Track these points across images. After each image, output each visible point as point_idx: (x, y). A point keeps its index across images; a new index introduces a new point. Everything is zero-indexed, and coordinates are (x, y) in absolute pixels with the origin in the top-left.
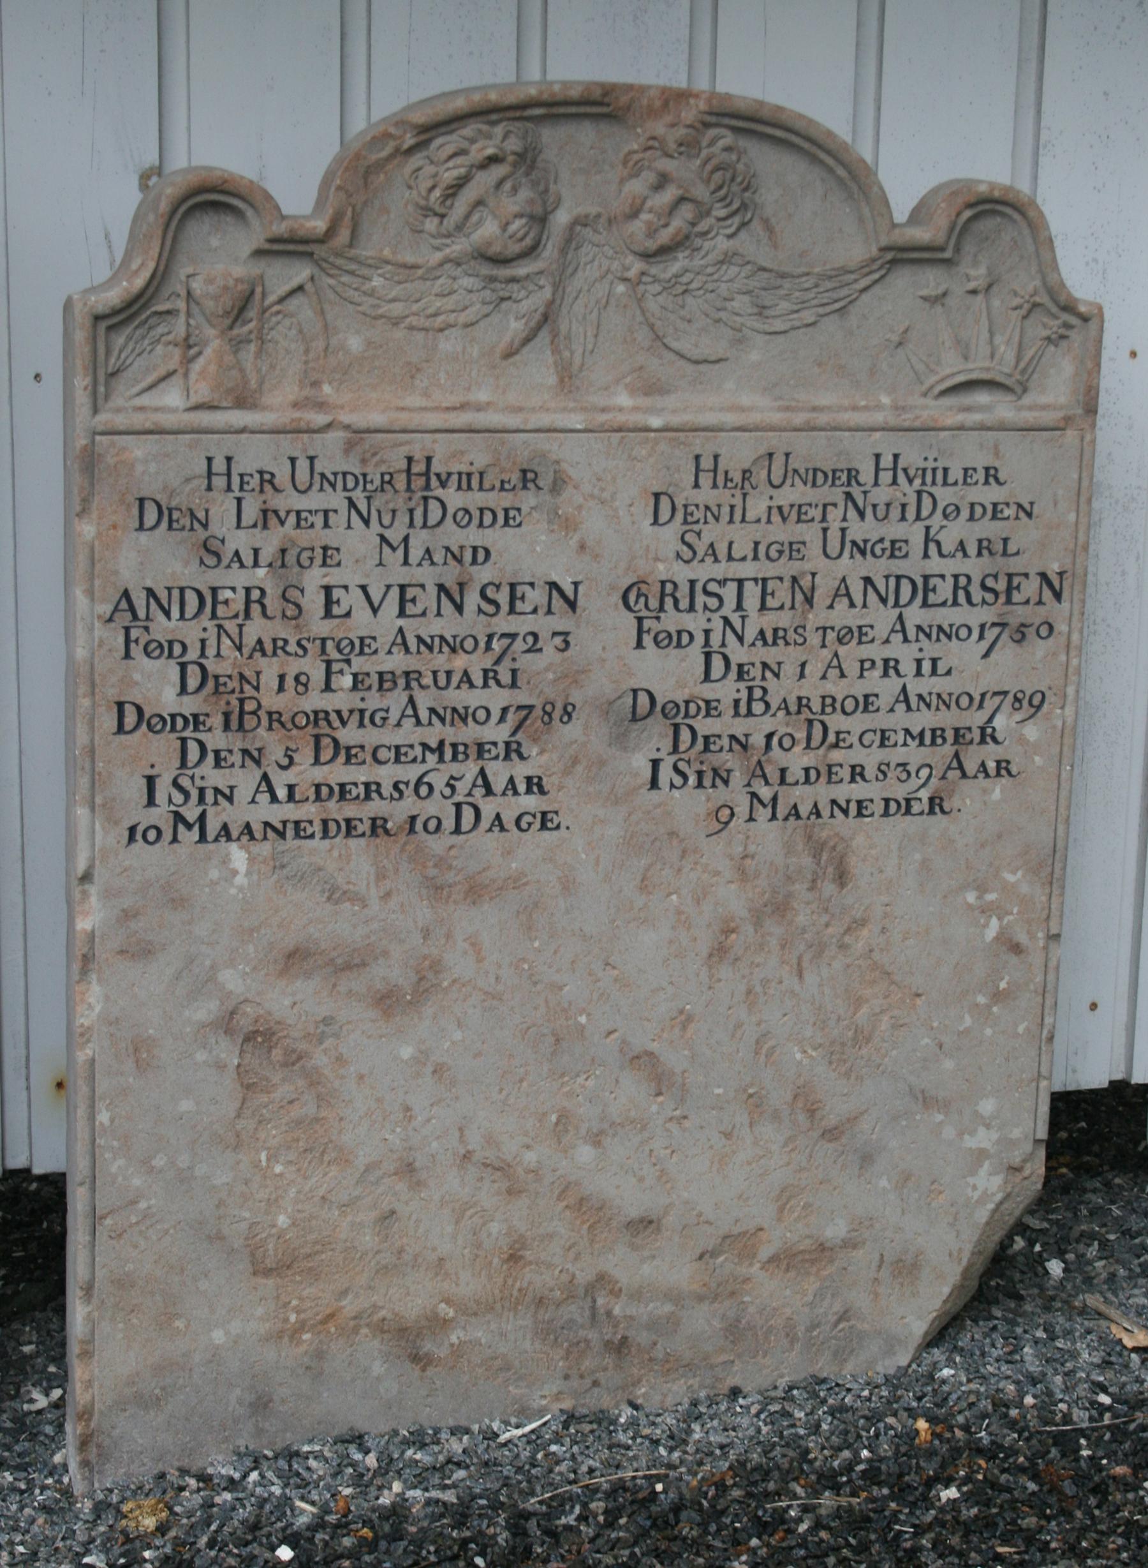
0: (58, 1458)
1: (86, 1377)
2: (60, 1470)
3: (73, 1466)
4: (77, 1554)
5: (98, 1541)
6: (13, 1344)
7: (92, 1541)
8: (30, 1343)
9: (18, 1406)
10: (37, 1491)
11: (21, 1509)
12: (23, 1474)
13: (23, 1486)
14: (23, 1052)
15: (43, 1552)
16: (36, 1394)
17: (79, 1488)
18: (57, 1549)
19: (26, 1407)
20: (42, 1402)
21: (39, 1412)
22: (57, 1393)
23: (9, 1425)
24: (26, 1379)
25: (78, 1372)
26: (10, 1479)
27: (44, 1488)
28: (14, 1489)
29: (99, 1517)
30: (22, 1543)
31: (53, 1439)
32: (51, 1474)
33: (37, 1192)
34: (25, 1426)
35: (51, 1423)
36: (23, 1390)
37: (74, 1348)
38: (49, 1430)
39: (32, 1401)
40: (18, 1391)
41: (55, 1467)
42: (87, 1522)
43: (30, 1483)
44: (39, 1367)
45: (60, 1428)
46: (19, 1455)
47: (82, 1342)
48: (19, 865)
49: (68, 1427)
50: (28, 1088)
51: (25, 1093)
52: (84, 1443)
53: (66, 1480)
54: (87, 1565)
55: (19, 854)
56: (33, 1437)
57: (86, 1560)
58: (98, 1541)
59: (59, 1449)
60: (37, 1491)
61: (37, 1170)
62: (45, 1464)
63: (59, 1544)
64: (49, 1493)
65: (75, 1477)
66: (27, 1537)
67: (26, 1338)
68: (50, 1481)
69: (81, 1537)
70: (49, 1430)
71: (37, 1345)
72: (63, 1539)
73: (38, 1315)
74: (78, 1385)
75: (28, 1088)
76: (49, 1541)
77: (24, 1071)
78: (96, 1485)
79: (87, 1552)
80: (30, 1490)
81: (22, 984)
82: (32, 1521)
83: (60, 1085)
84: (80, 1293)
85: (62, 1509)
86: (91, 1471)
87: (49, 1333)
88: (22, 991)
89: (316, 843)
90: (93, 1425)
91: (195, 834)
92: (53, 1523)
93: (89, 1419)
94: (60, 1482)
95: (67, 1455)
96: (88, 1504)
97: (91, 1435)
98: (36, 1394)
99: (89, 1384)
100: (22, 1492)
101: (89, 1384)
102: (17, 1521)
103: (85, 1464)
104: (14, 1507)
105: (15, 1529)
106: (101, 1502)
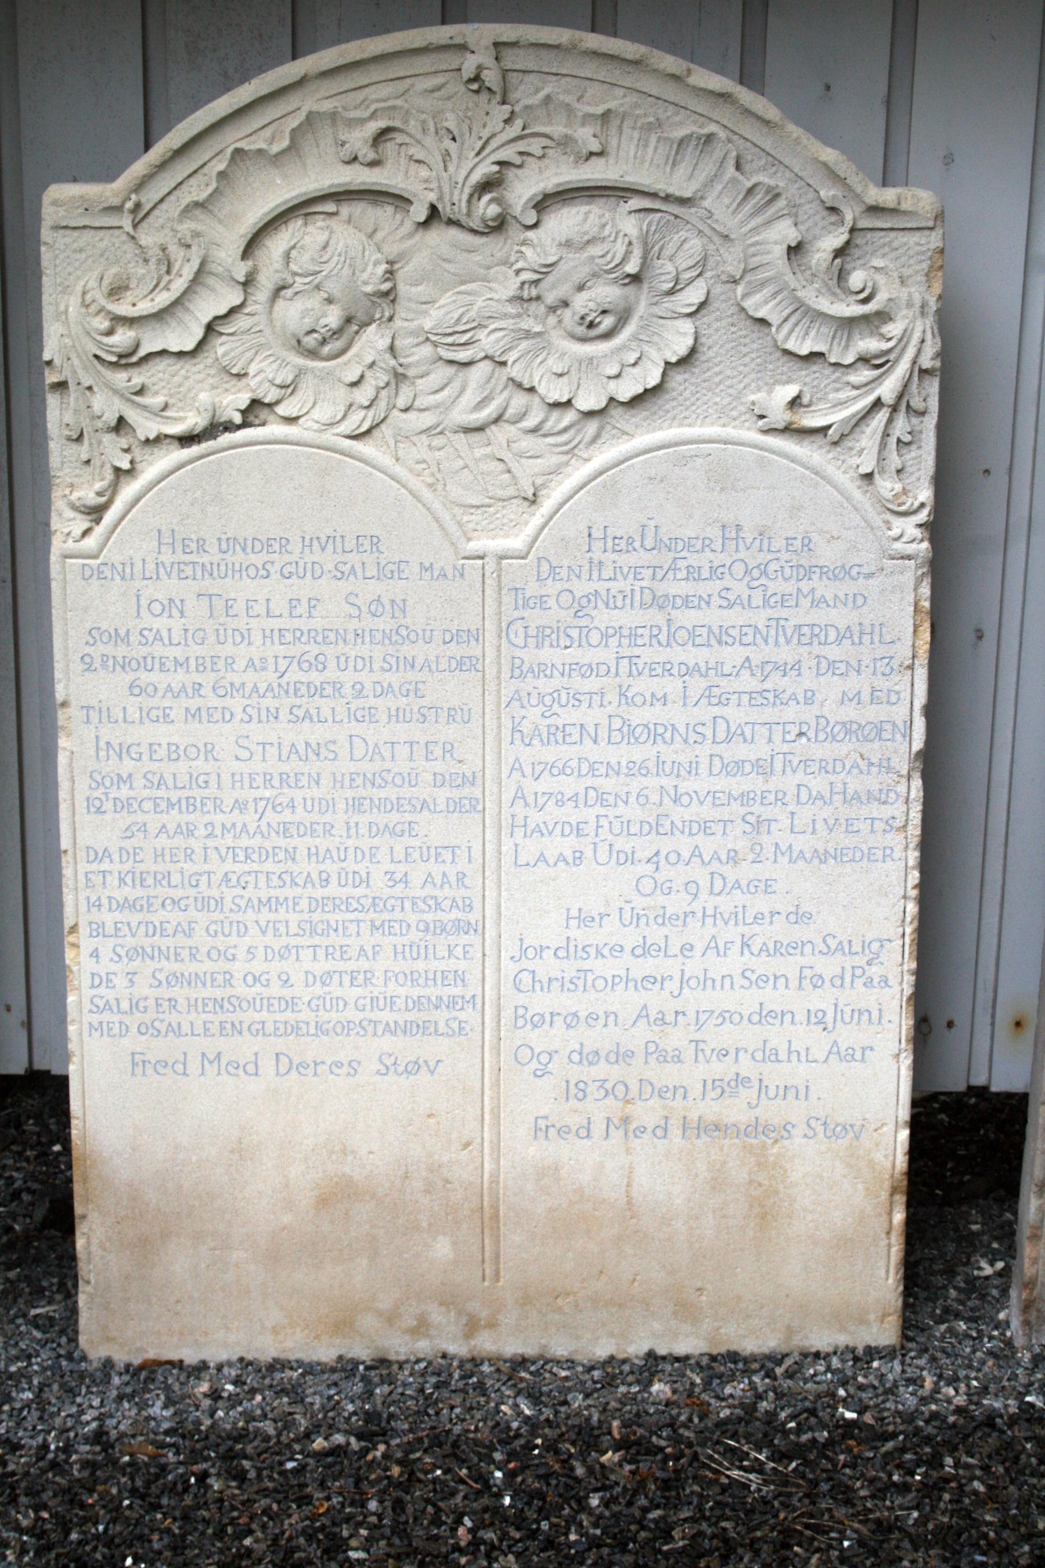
0: (1002, 1316)
1: (1033, 1255)
2: (1004, 1326)
3: (1015, 1323)
4: (1020, 1393)
5: (1036, 1385)
6: (963, 1222)
7: (1031, 1384)
8: (976, 1223)
9: (969, 1271)
10: (986, 1340)
11: (974, 1352)
12: (975, 1325)
13: (974, 1334)
14: (991, 995)
15: (992, 1388)
16: (983, 1264)
17: (1019, 1342)
18: (1003, 1387)
19: (976, 1272)
20: (988, 1271)
21: (987, 1278)
22: (1000, 1265)
23: (962, 1285)
24: (975, 1251)
25: (1027, 1251)
26: (964, 1327)
27: (991, 1338)
28: (967, 1336)
29: (1037, 1366)
30: (976, 1379)
31: (998, 1301)
32: (996, 1328)
33: (976, 1105)
34: (975, 1287)
35: (997, 1287)
36: (973, 1259)
37: (1024, 1231)
38: (995, 1292)
39: (980, 1269)
40: (969, 1259)
41: (999, 1322)
42: (1026, 1369)
43: (980, 1333)
44: (985, 1242)
45: (1005, 1291)
46: (971, 1310)
47: (1032, 1227)
48: (1002, 849)
49: (1013, 1293)
50: (993, 1024)
51: (989, 1027)
52: (1027, 1307)
53: (1008, 1334)
54: (1028, 1403)
55: (1003, 840)
56: (983, 1297)
57: (1028, 1399)
58: (1036, 1385)
59: (1003, 1309)
60: (986, 1340)
61: (994, 1089)
62: (992, 1319)
63: (1006, 1383)
64: (995, 1342)
65: (1015, 1330)
66: (980, 1375)
67: (973, 1218)
68: (996, 1333)
69: (1023, 1379)
70: (995, 1292)
71: (983, 1224)
72: (1009, 1380)
73: (981, 1201)
74: (1027, 1261)
75: (993, 1024)
76: (998, 1380)
77: (990, 1010)
78: (1034, 1341)
79: (1028, 1393)
80: (980, 1337)
81: (995, 941)
82: (983, 1363)
83: (1018, 1024)
84: (1034, 1189)
85: (1006, 1356)
86: (1031, 1329)
87: (991, 1218)
88: (995, 947)
89: (879, 865)
90: (1035, 1293)
91: (787, 858)
92: (1000, 1367)
93: (1033, 1289)
94: (1003, 1334)
95: (1011, 1315)
96: (1027, 1356)
97: (1033, 1301)
98: (983, 1264)
99: (1035, 1261)
100: (974, 1339)
101: (1035, 1261)
102: (971, 1360)
103: (1026, 1323)
104: (968, 1350)
105: (970, 1367)
106: (1038, 1355)
